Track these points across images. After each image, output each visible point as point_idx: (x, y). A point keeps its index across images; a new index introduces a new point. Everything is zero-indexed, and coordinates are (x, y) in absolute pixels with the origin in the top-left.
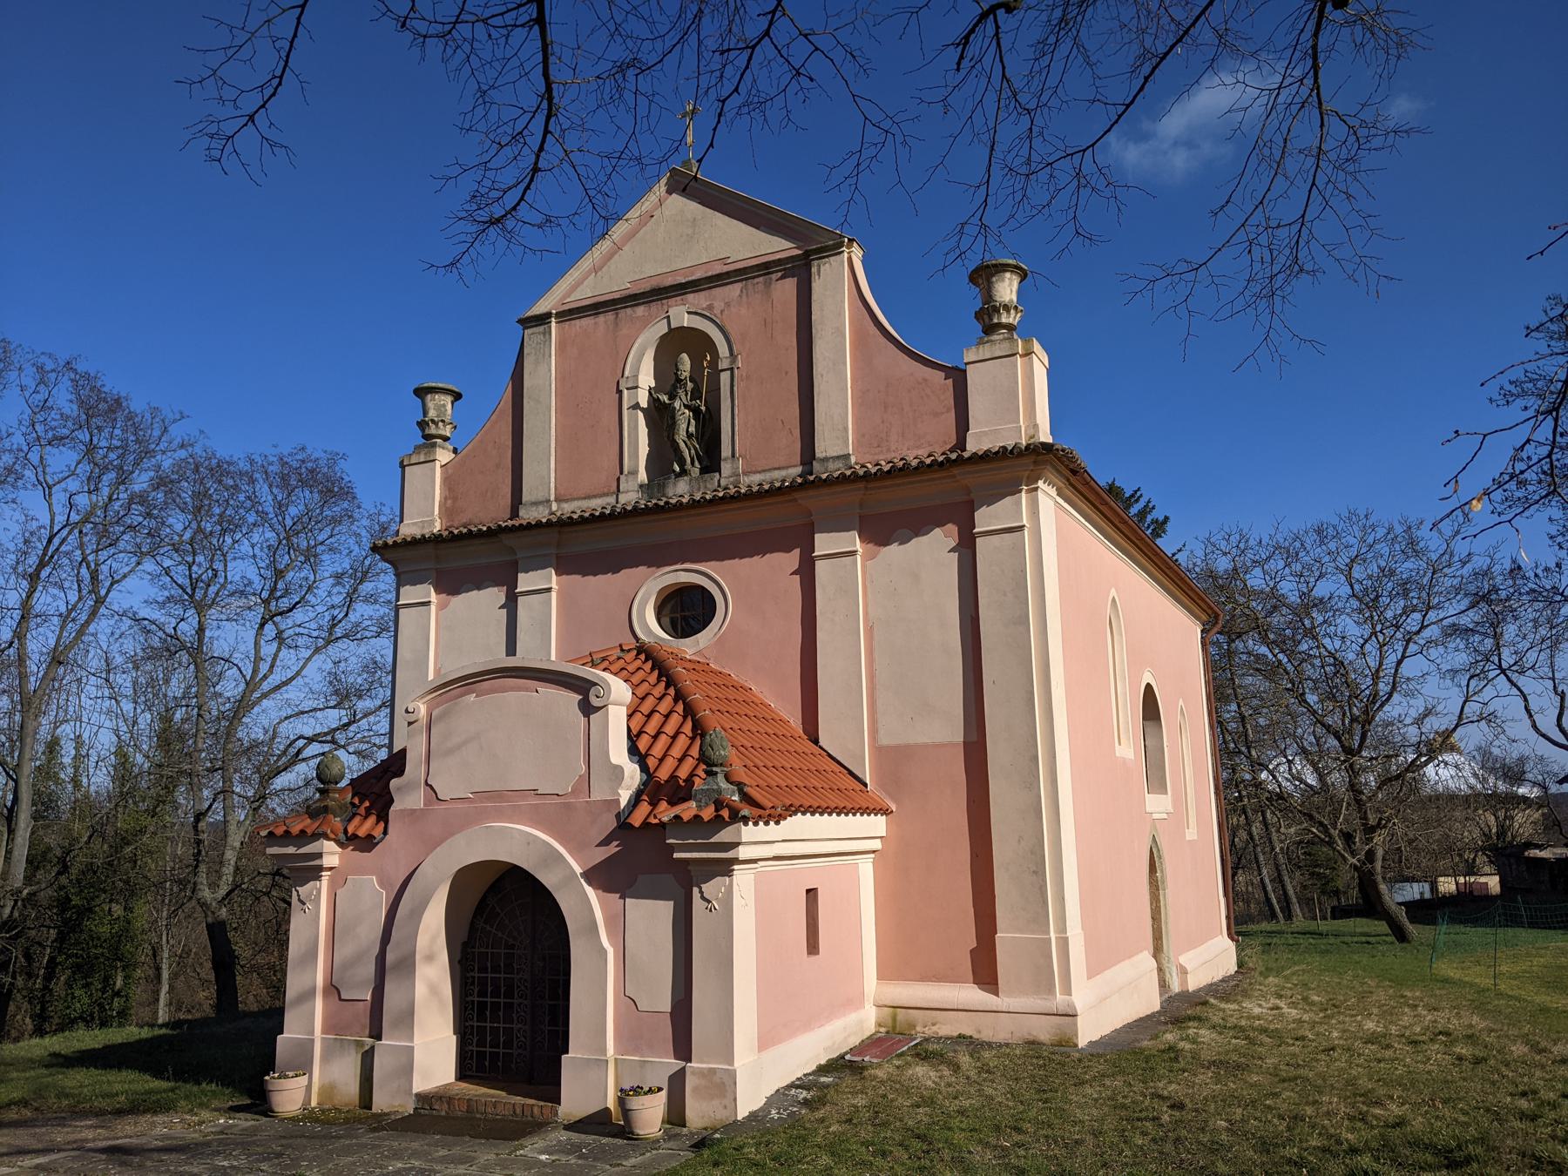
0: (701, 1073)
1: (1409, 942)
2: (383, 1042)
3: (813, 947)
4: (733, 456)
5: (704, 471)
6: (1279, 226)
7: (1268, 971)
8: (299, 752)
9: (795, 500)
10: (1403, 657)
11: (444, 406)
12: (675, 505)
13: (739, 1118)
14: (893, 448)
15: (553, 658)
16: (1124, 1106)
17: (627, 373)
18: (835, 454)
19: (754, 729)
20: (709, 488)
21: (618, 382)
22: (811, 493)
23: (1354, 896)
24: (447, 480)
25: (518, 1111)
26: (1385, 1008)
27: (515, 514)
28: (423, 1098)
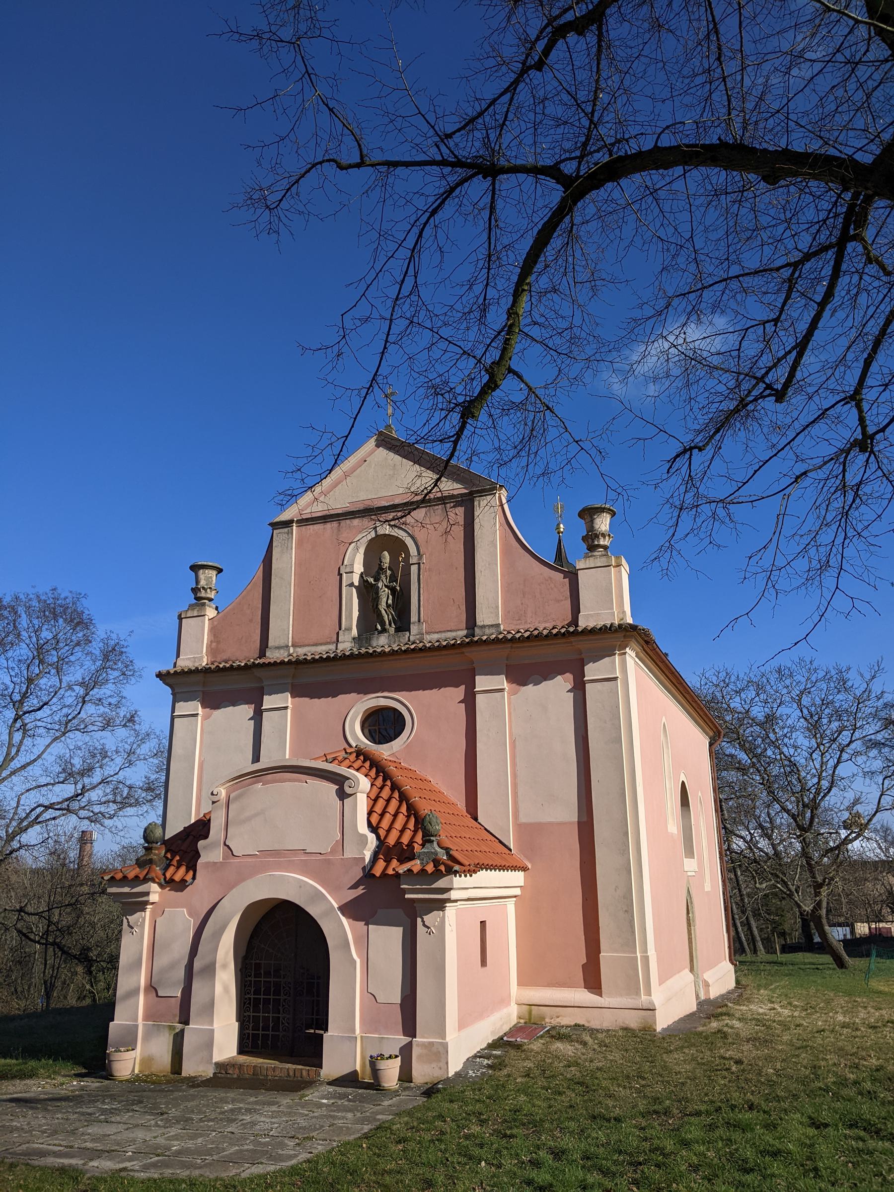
0: (423, 1045)
1: (846, 968)
2: (190, 1026)
3: (484, 963)
4: (419, 621)
5: (398, 630)
6: (820, 545)
7: (759, 987)
8: (38, 817)
9: (463, 653)
10: (839, 762)
11: (211, 577)
12: (380, 653)
13: (450, 1076)
14: (529, 621)
15: (287, 757)
16: (703, 1064)
17: (345, 563)
18: (490, 623)
19: (442, 811)
20: (401, 642)
21: (339, 568)
22: (474, 649)
23: (796, 935)
24: (213, 630)
25: (291, 1073)
26: (845, 1009)
27: (262, 654)
28: (218, 1065)
